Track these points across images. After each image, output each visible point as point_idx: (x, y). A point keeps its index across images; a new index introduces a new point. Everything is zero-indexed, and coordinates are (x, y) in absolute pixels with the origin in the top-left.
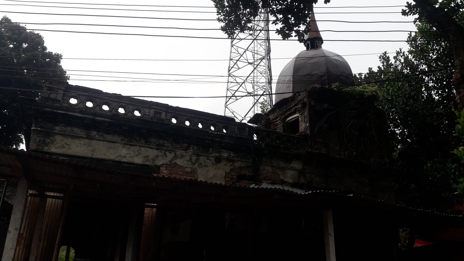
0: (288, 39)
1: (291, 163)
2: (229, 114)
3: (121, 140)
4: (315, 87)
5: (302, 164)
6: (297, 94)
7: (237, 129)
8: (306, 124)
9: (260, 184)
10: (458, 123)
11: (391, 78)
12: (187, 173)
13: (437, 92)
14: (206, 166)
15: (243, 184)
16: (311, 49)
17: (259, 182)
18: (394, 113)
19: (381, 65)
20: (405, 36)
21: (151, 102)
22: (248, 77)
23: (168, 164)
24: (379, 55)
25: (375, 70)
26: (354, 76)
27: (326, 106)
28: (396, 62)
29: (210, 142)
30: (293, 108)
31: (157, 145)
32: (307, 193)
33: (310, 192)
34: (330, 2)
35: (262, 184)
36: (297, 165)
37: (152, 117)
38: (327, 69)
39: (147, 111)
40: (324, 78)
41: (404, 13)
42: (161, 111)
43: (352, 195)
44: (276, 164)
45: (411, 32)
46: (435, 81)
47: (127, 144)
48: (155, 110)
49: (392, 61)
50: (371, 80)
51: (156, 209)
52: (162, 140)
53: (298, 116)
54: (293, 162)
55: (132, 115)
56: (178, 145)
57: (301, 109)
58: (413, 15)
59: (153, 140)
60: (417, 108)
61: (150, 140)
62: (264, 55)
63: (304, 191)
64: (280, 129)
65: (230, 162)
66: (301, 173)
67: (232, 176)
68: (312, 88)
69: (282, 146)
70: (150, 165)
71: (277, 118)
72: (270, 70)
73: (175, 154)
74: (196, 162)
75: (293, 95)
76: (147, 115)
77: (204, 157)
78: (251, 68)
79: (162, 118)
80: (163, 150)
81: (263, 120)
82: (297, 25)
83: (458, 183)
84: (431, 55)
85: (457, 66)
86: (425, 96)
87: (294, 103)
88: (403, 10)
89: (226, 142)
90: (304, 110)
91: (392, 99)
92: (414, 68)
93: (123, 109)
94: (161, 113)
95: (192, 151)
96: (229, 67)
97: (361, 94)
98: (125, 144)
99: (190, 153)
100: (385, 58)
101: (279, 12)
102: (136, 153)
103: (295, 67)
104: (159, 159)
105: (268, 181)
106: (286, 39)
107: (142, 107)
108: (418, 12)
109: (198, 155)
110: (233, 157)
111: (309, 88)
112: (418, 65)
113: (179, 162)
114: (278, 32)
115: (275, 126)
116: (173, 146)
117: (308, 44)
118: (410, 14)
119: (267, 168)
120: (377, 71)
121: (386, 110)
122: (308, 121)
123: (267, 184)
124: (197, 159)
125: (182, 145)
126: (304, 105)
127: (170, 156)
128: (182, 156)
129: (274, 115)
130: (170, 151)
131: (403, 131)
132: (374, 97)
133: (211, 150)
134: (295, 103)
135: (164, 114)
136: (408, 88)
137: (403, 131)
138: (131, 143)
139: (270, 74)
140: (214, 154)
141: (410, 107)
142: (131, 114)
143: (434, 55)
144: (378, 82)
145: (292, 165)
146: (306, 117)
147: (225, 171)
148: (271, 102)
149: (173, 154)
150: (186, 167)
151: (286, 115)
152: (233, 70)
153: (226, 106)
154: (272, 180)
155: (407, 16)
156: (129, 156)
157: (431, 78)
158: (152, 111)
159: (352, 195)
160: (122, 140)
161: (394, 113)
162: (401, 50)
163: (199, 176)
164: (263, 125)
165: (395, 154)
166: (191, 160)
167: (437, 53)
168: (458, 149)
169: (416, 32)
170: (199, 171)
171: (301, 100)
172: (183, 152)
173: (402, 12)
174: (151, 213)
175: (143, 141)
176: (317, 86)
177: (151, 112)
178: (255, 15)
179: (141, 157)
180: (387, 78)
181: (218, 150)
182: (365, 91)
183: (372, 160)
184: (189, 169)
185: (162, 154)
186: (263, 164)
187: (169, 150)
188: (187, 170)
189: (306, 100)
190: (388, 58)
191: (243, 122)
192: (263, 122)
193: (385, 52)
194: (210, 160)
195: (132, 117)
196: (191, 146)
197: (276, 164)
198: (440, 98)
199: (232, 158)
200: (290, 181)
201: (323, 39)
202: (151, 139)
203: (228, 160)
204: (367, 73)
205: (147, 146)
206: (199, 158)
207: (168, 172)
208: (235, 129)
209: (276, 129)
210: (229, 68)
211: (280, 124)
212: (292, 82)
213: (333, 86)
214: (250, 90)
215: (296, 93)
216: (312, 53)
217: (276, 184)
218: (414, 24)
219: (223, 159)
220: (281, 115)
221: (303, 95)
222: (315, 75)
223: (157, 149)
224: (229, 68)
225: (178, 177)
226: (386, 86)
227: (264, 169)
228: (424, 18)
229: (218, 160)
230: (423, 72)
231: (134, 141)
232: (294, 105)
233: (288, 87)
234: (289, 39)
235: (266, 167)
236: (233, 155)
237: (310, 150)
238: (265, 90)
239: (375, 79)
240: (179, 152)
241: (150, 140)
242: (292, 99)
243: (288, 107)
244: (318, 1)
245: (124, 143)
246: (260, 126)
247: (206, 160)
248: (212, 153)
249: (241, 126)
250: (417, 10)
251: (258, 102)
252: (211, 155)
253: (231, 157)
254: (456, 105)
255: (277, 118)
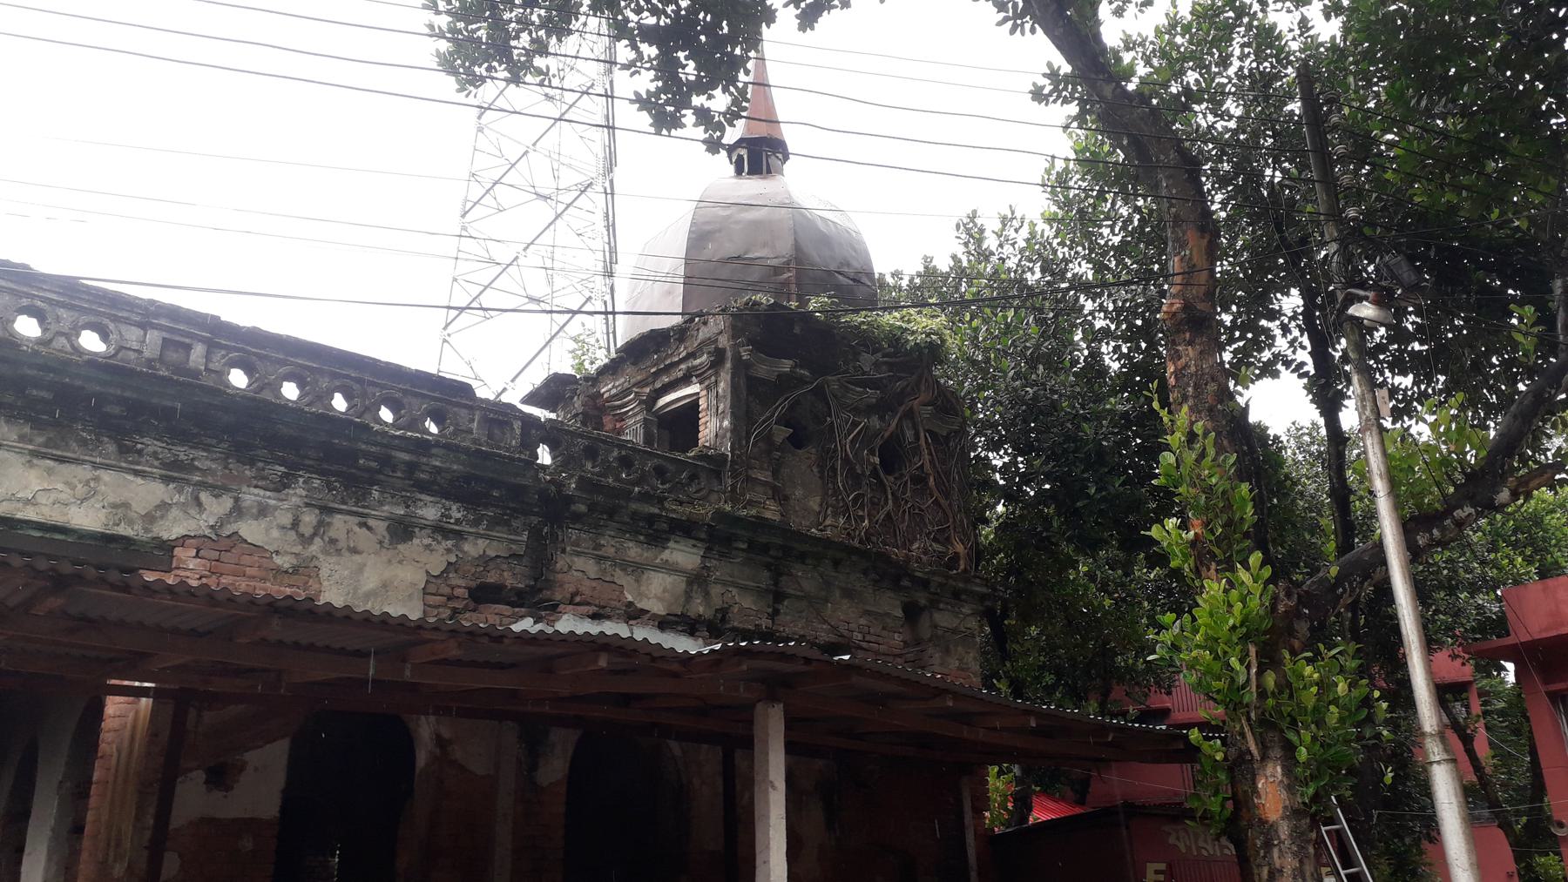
0: (669, 132)
1: (665, 548)
2: (453, 369)
3: (19, 437)
4: (756, 303)
5: (702, 553)
6: (697, 319)
7: (479, 422)
8: (721, 422)
9: (552, 618)
10: (1167, 447)
11: (986, 293)
12: (279, 572)
13: (1117, 349)
14: (354, 551)
15: (488, 617)
16: (748, 174)
17: (550, 609)
18: (989, 404)
19: (960, 251)
20: (1036, 170)
21: (152, 302)
22: (529, 245)
23: (205, 536)
24: (955, 221)
25: (943, 264)
26: (879, 280)
27: (786, 365)
28: (1001, 246)
29: (374, 464)
30: (683, 366)
31: (165, 465)
32: (706, 650)
33: (718, 647)
34: (812, 28)
35: (558, 620)
36: (684, 555)
37: (149, 361)
38: (797, 247)
39: (132, 335)
40: (786, 276)
41: (1038, 95)
42: (187, 341)
43: (847, 657)
44: (613, 550)
45: (1053, 157)
46: (1111, 313)
47: (44, 456)
48: (165, 335)
49: (991, 242)
50: (927, 294)
51: (151, 700)
52: (186, 448)
53: (698, 393)
54: (671, 544)
55: (72, 346)
56: (248, 467)
57: (709, 369)
58: (1062, 105)
59: (151, 445)
60: (1055, 392)
61: (139, 446)
62: (594, 175)
63: (700, 641)
64: (633, 432)
65: (446, 538)
66: (697, 581)
67: (453, 589)
68: (747, 304)
69: (636, 489)
70: (134, 540)
71: (626, 393)
72: (611, 227)
73: (237, 500)
74: (315, 534)
75: (685, 322)
76: (134, 350)
77: (348, 518)
78: (545, 212)
79: (191, 364)
80: (188, 482)
81: (576, 398)
82: (702, 87)
83: (1161, 627)
84: (1105, 231)
85: (1174, 275)
86: (1082, 358)
87: (685, 348)
88: (1034, 84)
89: (435, 467)
90: (717, 374)
91: (987, 360)
92: (1054, 269)
93: (34, 322)
94: (188, 348)
95: (304, 493)
96: (466, 201)
97: (895, 338)
98: (35, 454)
99: (294, 499)
100: (972, 232)
101: (649, 35)
102: (81, 490)
103: (694, 229)
104: (170, 518)
105: (582, 608)
106: (665, 132)
107: (115, 319)
108: (1077, 99)
109: (326, 510)
110: (458, 522)
111: (736, 302)
112: (1066, 261)
113: (250, 530)
114: (643, 102)
115: (617, 421)
116: (227, 471)
117: (740, 158)
118: (1055, 101)
119: (579, 562)
120: (948, 270)
121: (969, 393)
122: (728, 411)
123: (577, 618)
124: (321, 524)
125: (263, 469)
126: (718, 358)
127: (216, 507)
128: (263, 511)
129: (617, 384)
130: (218, 490)
131: (1014, 462)
132: (933, 351)
133: (376, 494)
134: (690, 350)
135: (198, 351)
136: (1034, 330)
137: (1014, 462)
138: (59, 453)
139: (612, 240)
140: (386, 508)
141: (1035, 388)
142: (65, 341)
143: (1114, 235)
144: (950, 304)
145: (666, 555)
146: (724, 397)
147: (427, 572)
148: (611, 335)
149: (227, 503)
150: (277, 552)
151: (658, 385)
152: (478, 212)
153: (447, 338)
154: (596, 606)
155: (1047, 105)
156: (51, 500)
157: (1101, 305)
158: (154, 337)
159: (847, 657)
160: (22, 438)
161: (989, 404)
162: (1013, 213)
163: (325, 583)
164: (576, 415)
165: (987, 533)
166: (298, 524)
167: (1123, 228)
168: (1164, 527)
169: (1067, 160)
170: (327, 565)
171: (709, 339)
172: (268, 493)
173: (1030, 92)
174: (131, 715)
175: (111, 448)
176: (764, 301)
177: (147, 341)
178: (562, 31)
179: (98, 506)
180: (973, 295)
181: (404, 493)
182: (907, 329)
183: (916, 545)
184: (287, 558)
185: (182, 499)
186: (568, 549)
187: (214, 487)
188: (278, 560)
189: (724, 341)
190: (982, 231)
191: (505, 399)
192: (578, 403)
193: (974, 212)
194: (369, 528)
195: (71, 354)
196: (301, 476)
197: (613, 550)
198: (1123, 366)
199: (456, 524)
200: (658, 608)
201: (790, 151)
202: (144, 440)
203: (440, 530)
204: (919, 275)
205: (124, 465)
206: (328, 520)
207: (204, 566)
208: (473, 420)
209: (620, 432)
210: (464, 206)
211: (635, 415)
212: (682, 281)
213: (813, 304)
214: (538, 288)
215: (692, 318)
216: (752, 187)
217: (609, 618)
218: (1064, 132)
219: (421, 529)
220: (640, 384)
221: (715, 327)
222: (757, 262)
223: (166, 480)
224: (464, 206)
225: (242, 585)
226: (972, 319)
227: (570, 567)
228: (1094, 117)
229: (402, 531)
230: (1080, 285)
231: (74, 444)
232: (684, 354)
233: (669, 293)
234: (673, 132)
235: (576, 559)
236: (459, 515)
237: (728, 508)
238: (593, 295)
239: (941, 294)
240: (251, 496)
241: (139, 446)
242: (680, 334)
243: (665, 359)
244: (819, 20)
245: (30, 450)
246: (565, 417)
247: (357, 529)
248: (381, 503)
249: (498, 415)
250: (1074, 90)
251: (564, 335)
252: (373, 513)
253: (452, 521)
254: (1163, 390)
255: (626, 393)
